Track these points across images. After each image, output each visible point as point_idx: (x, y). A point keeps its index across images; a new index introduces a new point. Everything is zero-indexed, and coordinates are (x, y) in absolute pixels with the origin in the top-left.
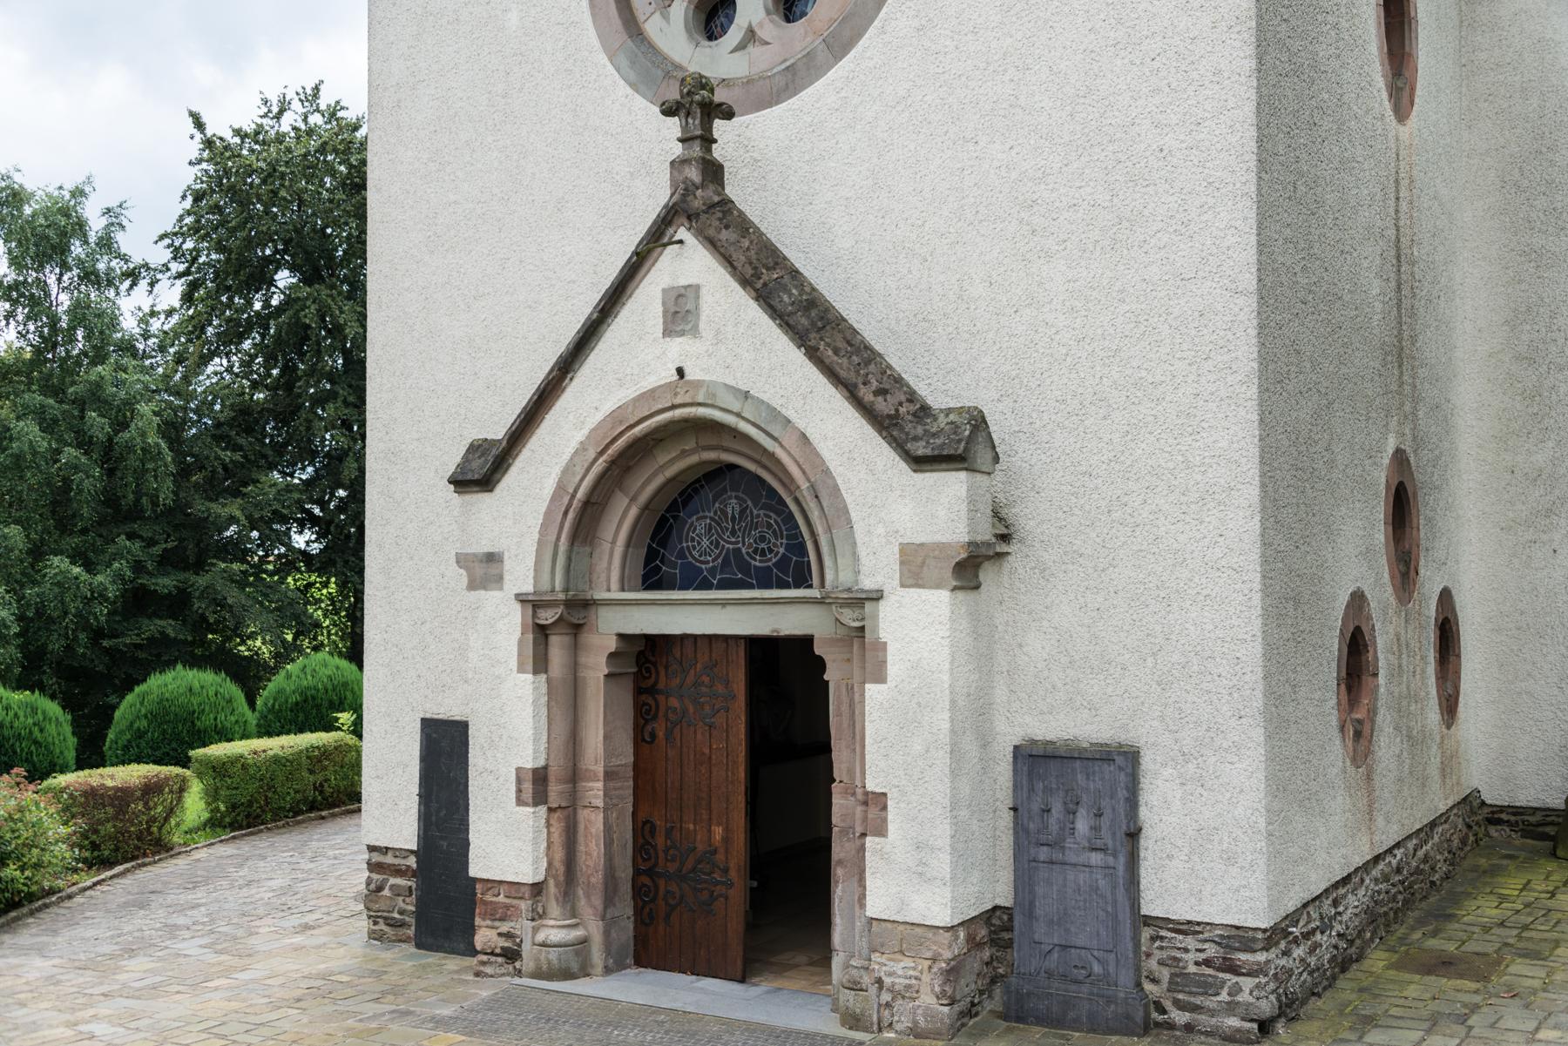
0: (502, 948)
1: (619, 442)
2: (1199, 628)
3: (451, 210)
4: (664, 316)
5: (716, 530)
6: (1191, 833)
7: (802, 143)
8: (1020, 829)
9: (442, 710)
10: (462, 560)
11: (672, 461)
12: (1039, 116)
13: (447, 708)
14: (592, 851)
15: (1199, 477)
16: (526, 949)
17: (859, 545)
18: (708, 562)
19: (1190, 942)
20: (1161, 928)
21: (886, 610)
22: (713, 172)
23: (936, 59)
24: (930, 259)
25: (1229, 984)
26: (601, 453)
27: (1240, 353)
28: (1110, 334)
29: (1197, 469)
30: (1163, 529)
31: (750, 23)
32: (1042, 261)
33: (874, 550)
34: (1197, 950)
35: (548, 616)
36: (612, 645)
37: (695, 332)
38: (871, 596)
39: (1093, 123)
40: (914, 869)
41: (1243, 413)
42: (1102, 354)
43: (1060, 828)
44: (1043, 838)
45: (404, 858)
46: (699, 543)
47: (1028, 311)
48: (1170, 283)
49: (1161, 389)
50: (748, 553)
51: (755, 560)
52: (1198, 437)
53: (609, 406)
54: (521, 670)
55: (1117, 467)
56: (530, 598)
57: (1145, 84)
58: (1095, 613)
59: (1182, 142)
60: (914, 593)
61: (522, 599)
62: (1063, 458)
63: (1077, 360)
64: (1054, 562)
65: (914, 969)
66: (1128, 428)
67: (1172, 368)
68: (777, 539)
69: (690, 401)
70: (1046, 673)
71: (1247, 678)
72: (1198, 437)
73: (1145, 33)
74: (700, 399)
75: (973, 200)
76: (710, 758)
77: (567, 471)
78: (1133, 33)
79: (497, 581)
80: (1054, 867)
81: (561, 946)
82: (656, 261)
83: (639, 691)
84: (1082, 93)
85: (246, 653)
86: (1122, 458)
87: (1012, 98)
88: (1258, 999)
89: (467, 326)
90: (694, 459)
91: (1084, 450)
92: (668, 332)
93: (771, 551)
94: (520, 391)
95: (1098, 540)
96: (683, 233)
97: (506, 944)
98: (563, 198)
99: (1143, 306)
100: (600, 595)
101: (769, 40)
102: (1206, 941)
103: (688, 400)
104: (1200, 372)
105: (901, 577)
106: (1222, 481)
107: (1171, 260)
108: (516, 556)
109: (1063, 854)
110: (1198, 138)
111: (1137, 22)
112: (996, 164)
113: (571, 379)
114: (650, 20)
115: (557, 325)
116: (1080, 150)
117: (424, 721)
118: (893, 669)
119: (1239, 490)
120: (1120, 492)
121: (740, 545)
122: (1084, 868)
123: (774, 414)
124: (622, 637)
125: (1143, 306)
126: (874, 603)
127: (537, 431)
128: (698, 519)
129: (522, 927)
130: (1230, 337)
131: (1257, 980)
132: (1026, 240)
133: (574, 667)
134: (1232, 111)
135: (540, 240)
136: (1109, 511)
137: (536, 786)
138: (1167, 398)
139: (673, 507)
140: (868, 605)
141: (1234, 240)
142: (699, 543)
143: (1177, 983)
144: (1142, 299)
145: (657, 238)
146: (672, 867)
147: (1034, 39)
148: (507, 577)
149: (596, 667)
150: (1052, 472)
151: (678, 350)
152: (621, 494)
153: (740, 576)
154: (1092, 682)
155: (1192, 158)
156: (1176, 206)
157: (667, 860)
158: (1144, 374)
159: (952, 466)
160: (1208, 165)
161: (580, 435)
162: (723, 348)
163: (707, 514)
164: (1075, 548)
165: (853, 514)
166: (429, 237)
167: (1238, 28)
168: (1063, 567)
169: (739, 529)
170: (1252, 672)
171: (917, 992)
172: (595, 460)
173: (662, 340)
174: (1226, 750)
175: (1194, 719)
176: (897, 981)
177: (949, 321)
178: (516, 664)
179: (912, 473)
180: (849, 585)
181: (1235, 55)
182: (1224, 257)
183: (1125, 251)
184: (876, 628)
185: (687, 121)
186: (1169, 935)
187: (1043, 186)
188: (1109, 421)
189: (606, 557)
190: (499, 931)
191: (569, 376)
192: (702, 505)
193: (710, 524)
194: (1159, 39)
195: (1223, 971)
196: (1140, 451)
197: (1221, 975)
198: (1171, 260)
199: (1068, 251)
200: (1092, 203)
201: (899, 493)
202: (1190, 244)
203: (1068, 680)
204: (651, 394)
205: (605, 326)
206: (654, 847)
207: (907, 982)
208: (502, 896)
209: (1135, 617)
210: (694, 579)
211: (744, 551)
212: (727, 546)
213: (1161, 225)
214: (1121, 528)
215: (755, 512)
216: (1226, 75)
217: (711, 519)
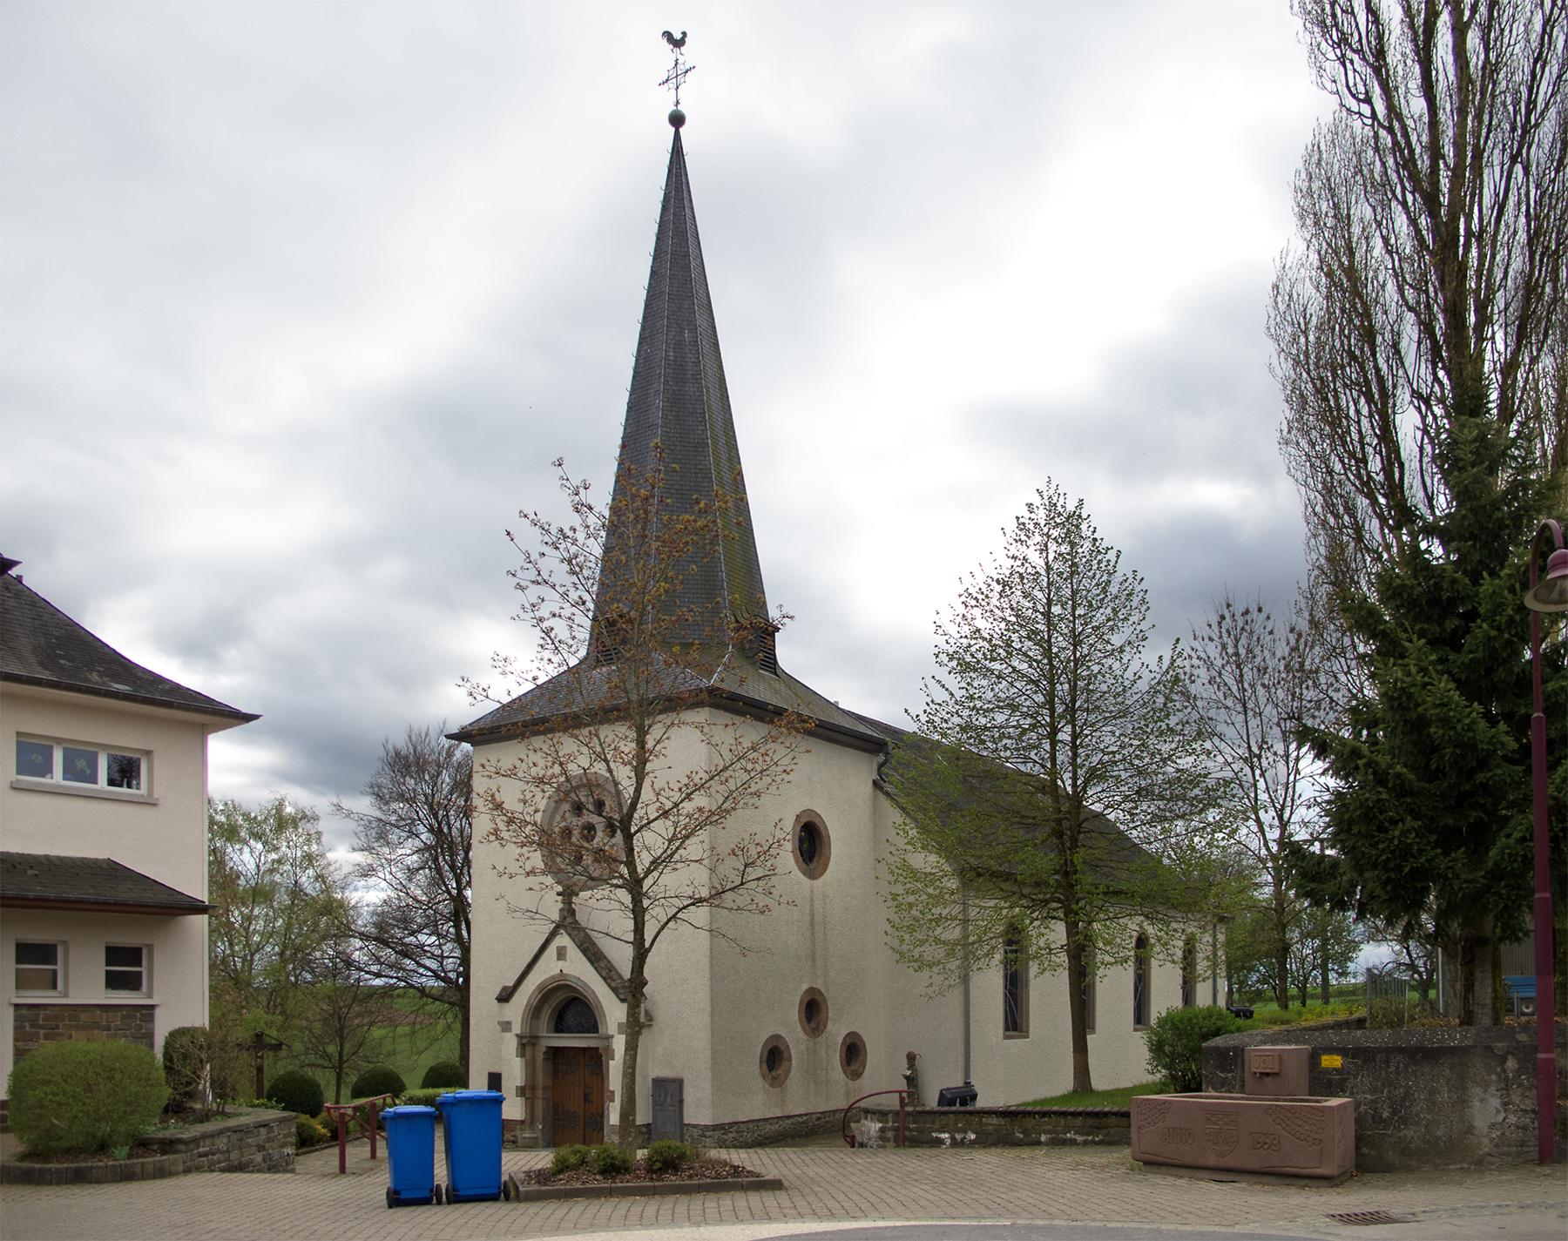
8: (654, 1101)
10: (499, 1023)
13: (495, 1070)
14: (539, 1112)
16: (519, 1139)
22: (573, 913)
35: (525, 1041)
36: (544, 1049)
37: (565, 959)
61: (517, 1035)
77: (530, 997)
83: (554, 1064)
85: (1377, 417)
90: (568, 995)
92: (558, 959)
96: (562, 931)
117: (490, 1074)
124: (547, 1047)
129: (518, 1133)
133: (534, 1056)
137: (521, 1091)
139: (563, 1008)
145: (553, 934)
149: (540, 1057)
161: (534, 987)
204: (553, 977)
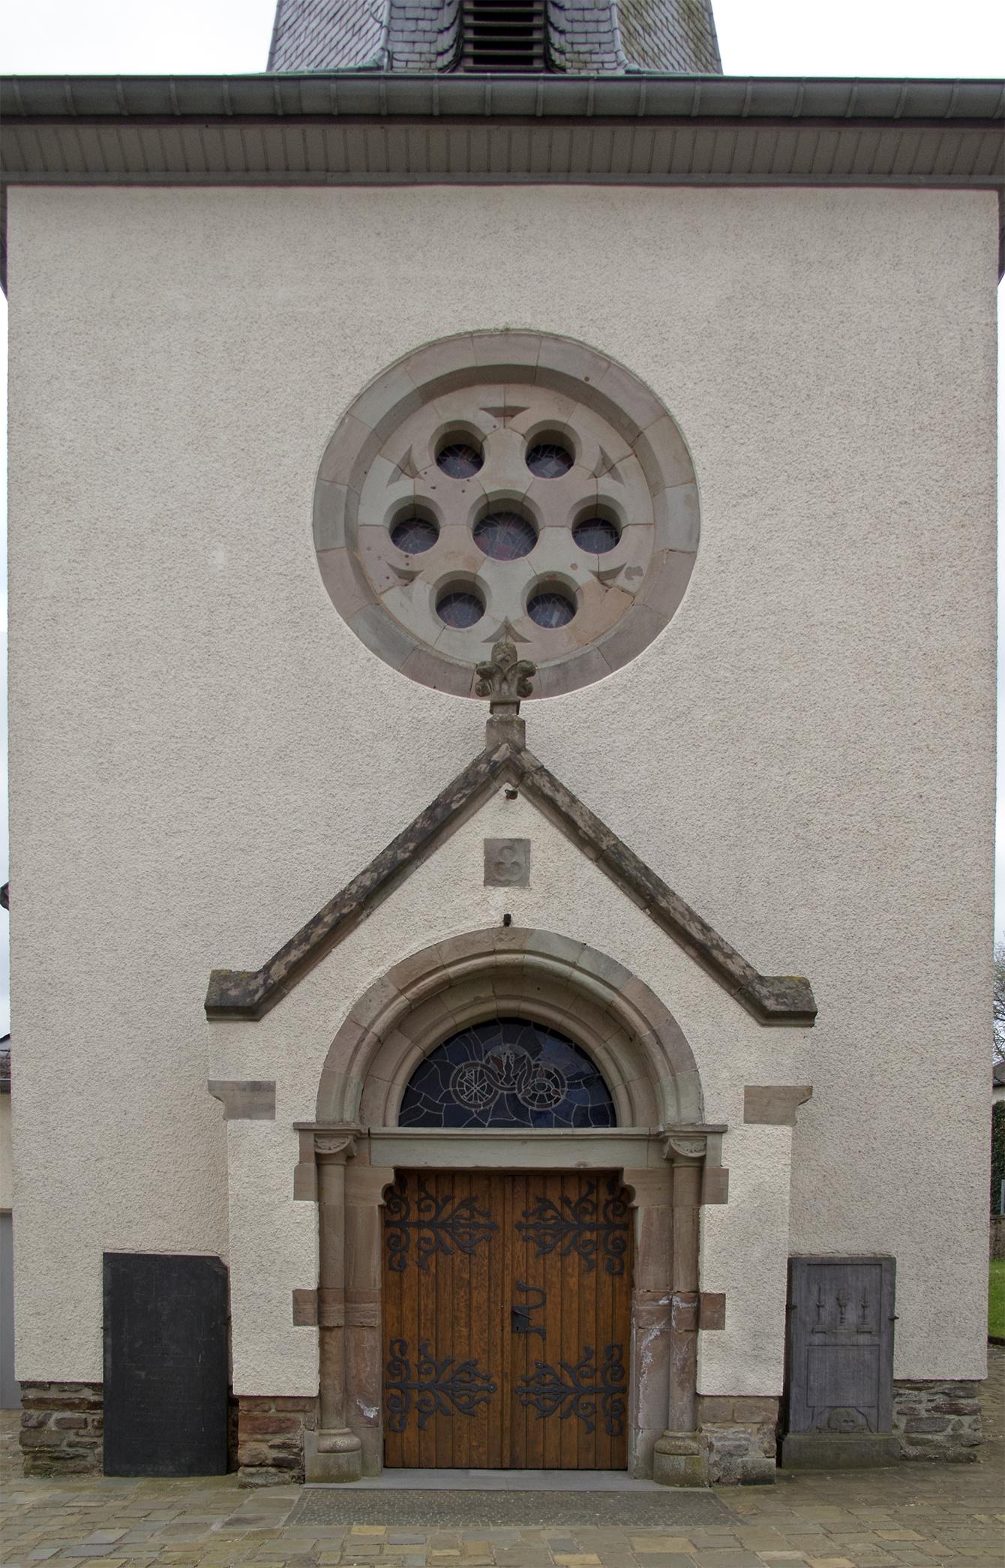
0: (274, 1459)
1: (427, 981)
2: (943, 1165)
3: (132, 740)
4: (486, 865)
5: (488, 1077)
6: (930, 1316)
7: (575, 736)
9: (128, 1245)
11: (464, 1008)
12: (814, 751)
15: (946, 1052)
17: (703, 1086)
18: (479, 1106)
19: (924, 1396)
20: (900, 1388)
21: (727, 1142)
23: (716, 686)
24: (709, 856)
25: (953, 1422)
26: (402, 992)
27: (980, 960)
28: (875, 936)
29: (945, 1046)
30: (916, 1090)
31: (506, 617)
32: (816, 871)
33: (719, 1091)
34: (929, 1401)
37: (523, 882)
38: (717, 1130)
39: (862, 765)
40: (750, 1353)
41: (982, 1006)
42: (868, 951)
43: (832, 1319)
44: (818, 1328)
45: (77, 1391)
46: (468, 1088)
47: (803, 910)
48: (927, 901)
49: (917, 982)
50: (524, 1099)
51: (533, 1105)
52: (946, 1022)
53: (415, 946)
54: (298, 1196)
55: (879, 1041)
56: (314, 1127)
57: (907, 742)
58: (857, 1155)
59: (938, 793)
60: (758, 1128)
61: (301, 1129)
62: (831, 1032)
63: (846, 954)
64: (822, 1114)
65: (744, 1432)
66: (888, 1011)
67: (926, 967)
68: (557, 1087)
69: (517, 948)
70: (812, 1202)
71: (978, 1202)
72: (946, 1022)
73: (908, 701)
74: (528, 947)
75: (751, 812)
76: (470, 1282)
78: (897, 699)
79: (268, 1110)
80: (827, 1348)
81: (348, 1451)
82: (476, 812)
84: (852, 740)
86: (883, 1035)
87: (789, 732)
88: (975, 1430)
89: (157, 861)
91: (851, 1026)
93: (550, 1097)
94: (228, 933)
95: (861, 1097)
97: (281, 1455)
98: (287, 747)
99: (904, 917)
100: (377, 1129)
101: (528, 638)
102: (937, 1393)
103: (512, 946)
104: (949, 972)
105: (745, 1115)
106: (964, 1056)
107: (928, 884)
108: (292, 1086)
109: (836, 1338)
110: (951, 792)
111: (902, 691)
112: (774, 784)
113: (368, 916)
114: (387, 593)
115: (279, 872)
116: (851, 786)
118: (736, 1190)
119: (977, 1063)
120: (880, 1061)
121: (516, 1091)
122: (852, 1348)
123: (613, 964)
125: (904, 917)
126: (717, 1136)
127: (321, 964)
128: (466, 1067)
130: (975, 948)
131: (975, 1417)
132: (802, 852)
134: (978, 776)
135: (256, 784)
136: (871, 1076)
138: (922, 990)
140: (710, 1139)
141: (979, 874)
142: (468, 1088)
143: (912, 1427)
144: (903, 911)
146: (426, 1380)
147: (811, 687)
148: (279, 1107)
150: (821, 1042)
151: (501, 899)
152: (400, 1035)
153: (515, 1119)
154: (853, 1208)
155: (946, 806)
156: (933, 841)
157: (420, 1373)
158: (903, 970)
159: (802, 1023)
160: (959, 814)
162: (556, 902)
163: (478, 1061)
164: (840, 1103)
165: (697, 1060)
166: (101, 763)
167: (984, 713)
168: (830, 1118)
169: (515, 1077)
170: (982, 1197)
171: (747, 1450)
172: (396, 997)
173: (482, 888)
174: (960, 1255)
175: (936, 1233)
176: (726, 1443)
177: (727, 911)
178: (292, 1190)
179: (759, 1028)
180: (692, 1121)
181: (981, 733)
182: (970, 886)
183: (890, 872)
184: (718, 1157)
185: (500, 687)
186: (907, 1392)
187: (817, 810)
188: (873, 1005)
189: (383, 1096)
190: (270, 1444)
191: (365, 913)
192: (471, 1051)
193: (481, 1071)
194: (919, 708)
195: (949, 1413)
196: (898, 1030)
197: (947, 1417)
198: (928, 884)
199: (839, 865)
200: (862, 829)
201: (745, 1043)
202: (943, 873)
203: (831, 1207)
205: (414, 867)
206: (406, 1363)
207: (738, 1443)
208: (273, 1411)
209: (891, 1157)
210: (457, 1118)
211: (519, 1096)
212: (500, 1092)
213: (919, 855)
214: (881, 1088)
215: (533, 1062)
216: (974, 747)
217: (482, 1066)
